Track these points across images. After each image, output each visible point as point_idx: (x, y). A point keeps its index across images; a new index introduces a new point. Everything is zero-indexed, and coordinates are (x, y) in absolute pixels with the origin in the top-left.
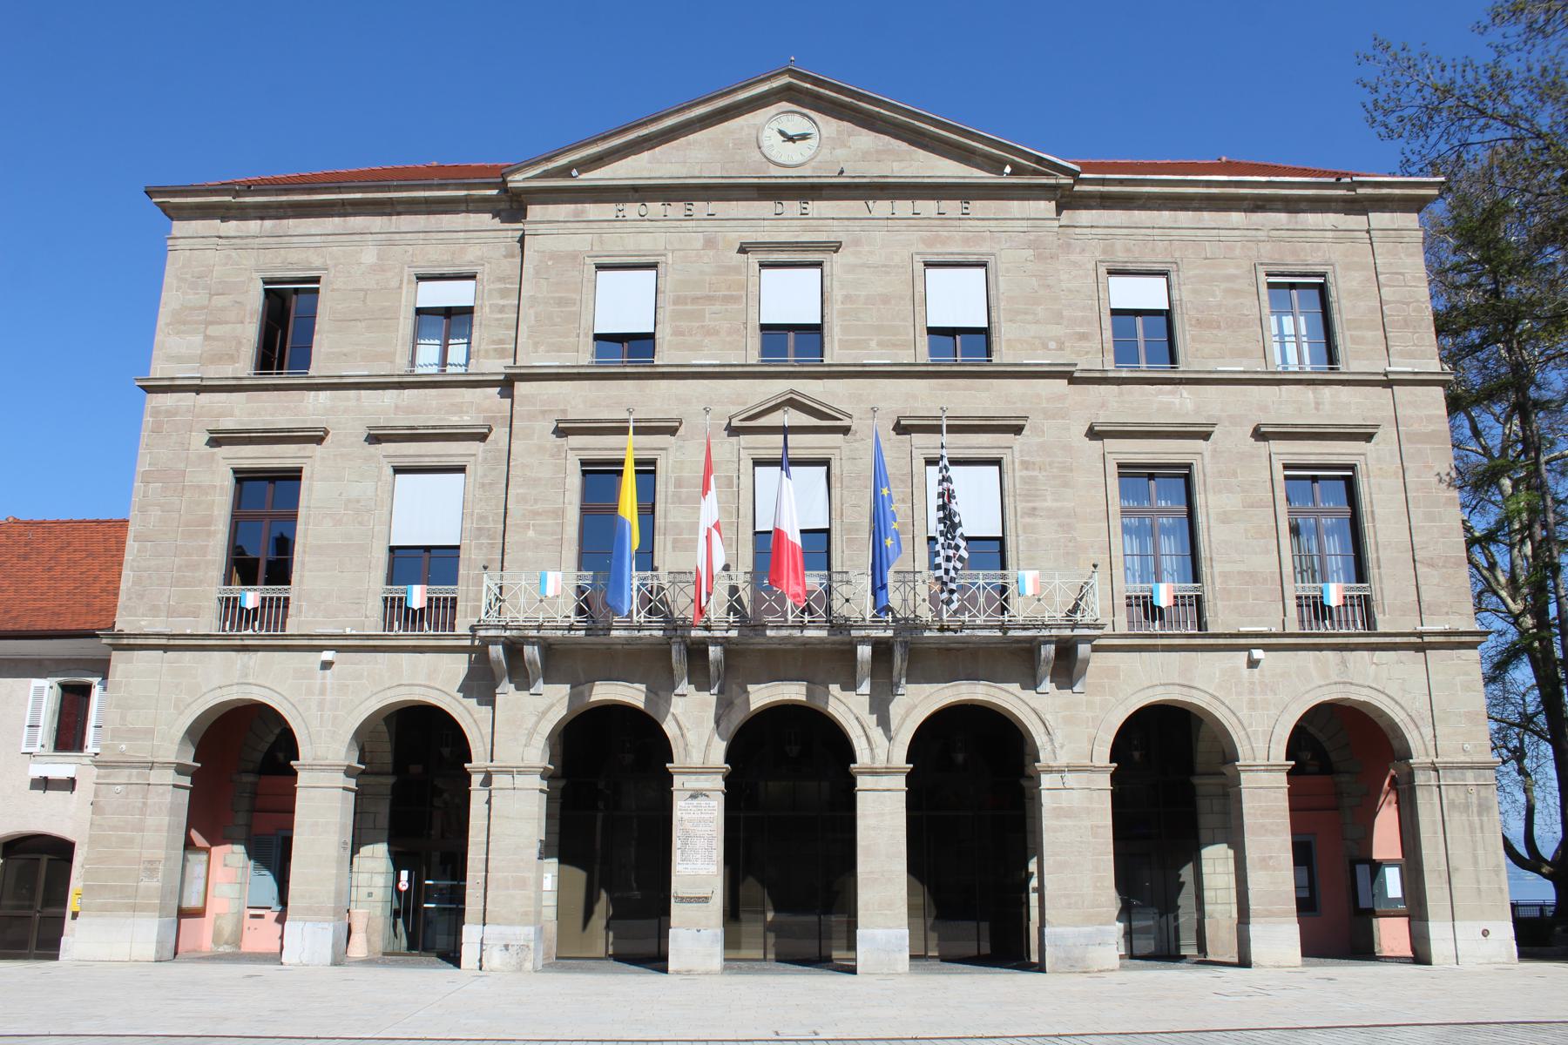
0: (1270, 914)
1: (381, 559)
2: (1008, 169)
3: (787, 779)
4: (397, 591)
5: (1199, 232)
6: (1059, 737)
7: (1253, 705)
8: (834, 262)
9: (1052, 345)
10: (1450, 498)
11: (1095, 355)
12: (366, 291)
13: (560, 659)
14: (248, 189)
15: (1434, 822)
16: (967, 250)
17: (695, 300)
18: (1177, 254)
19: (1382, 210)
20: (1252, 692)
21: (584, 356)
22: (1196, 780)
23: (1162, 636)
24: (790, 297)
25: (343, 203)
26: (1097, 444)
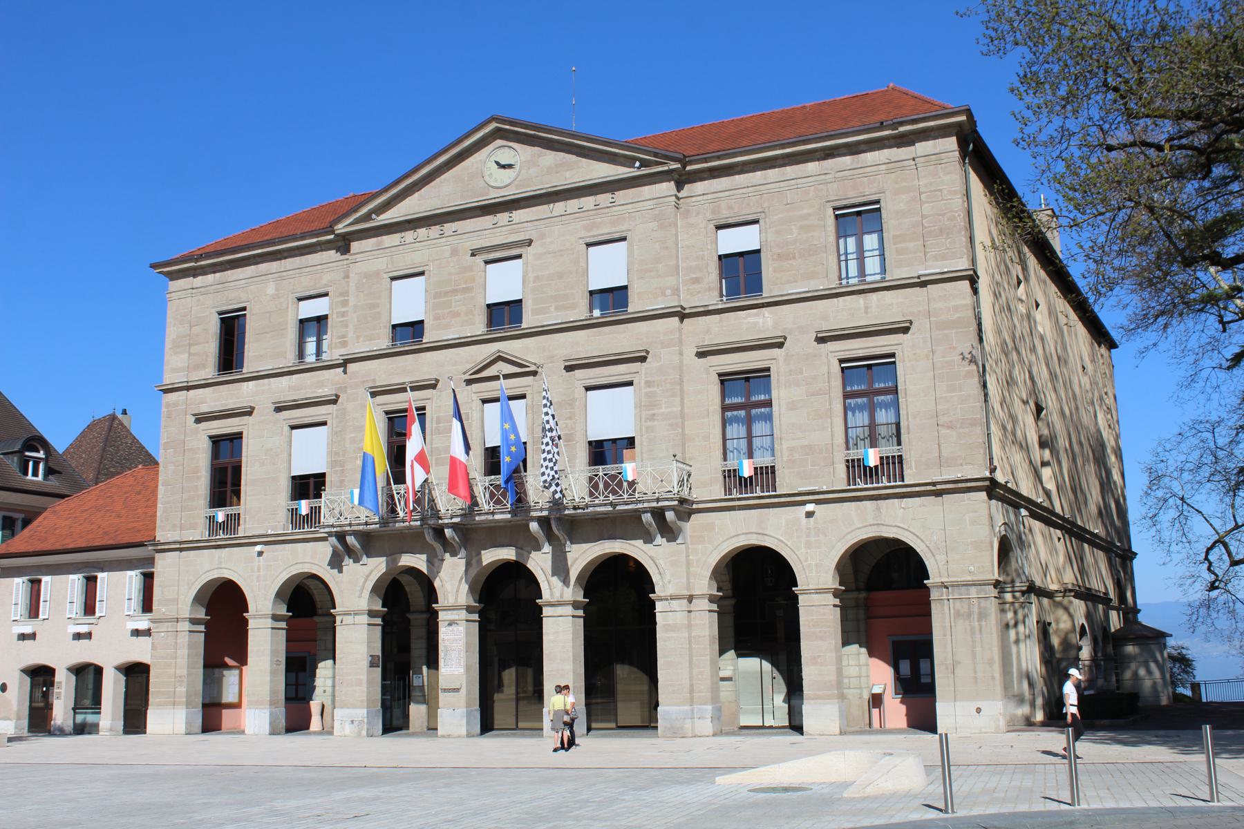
0: (817, 698)
1: (285, 487)
2: (637, 164)
3: (508, 610)
5: (782, 184)
6: (668, 576)
7: (809, 545)
8: (528, 252)
9: (669, 292)
10: (969, 372)
11: (708, 291)
13: (370, 542)
14: (201, 257)
15: (944, 628)
16: (613, 229)
18: (766, 205)
19: (927, 139)
20: (808, 536)
21: (580, 312)
22: (410, 616)
23: (739, 499)
24: (503, 283)
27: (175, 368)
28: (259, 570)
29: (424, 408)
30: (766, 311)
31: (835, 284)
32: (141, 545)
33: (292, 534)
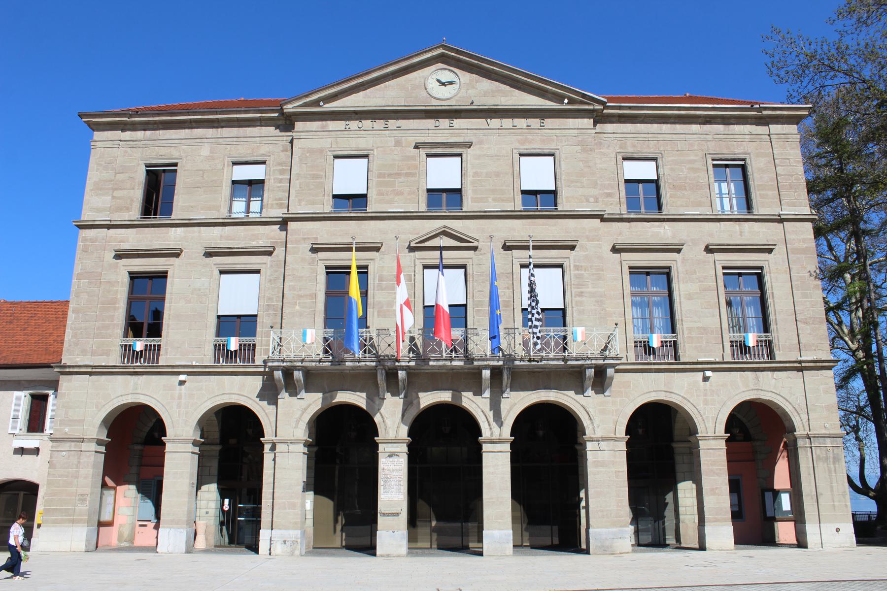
0: (716, 520)
1: (213, 323)
2: (566, 101)
4: (222, 340)
5: (674, 136)
6: (597, 421)
7: (706, 402)
8: (468, 153)
9: (592, 200)
10: (816, 285)
11: (616, 205)
12: (203, 171)
13: (313, 379)
14: (137, 113)
17: (390, 175)
18: (662, 149)
19: (777, 123)
20: (705, 395)
21: (327, 207)
22: (674, 445)
23: (654, 364)
24: (443, 173)
25: (191, 121)
26: (617, 255)
27: (95, 205)
28: (180, 398)
29: (366, 267)
30: (666, 225)
31: (226, 214)
32: (48, 366)
33: (222, 367)
